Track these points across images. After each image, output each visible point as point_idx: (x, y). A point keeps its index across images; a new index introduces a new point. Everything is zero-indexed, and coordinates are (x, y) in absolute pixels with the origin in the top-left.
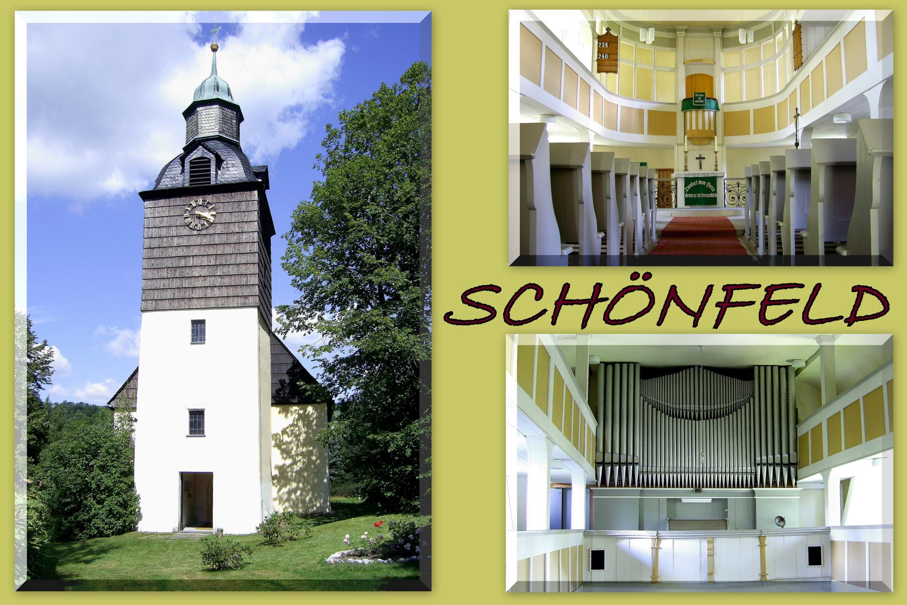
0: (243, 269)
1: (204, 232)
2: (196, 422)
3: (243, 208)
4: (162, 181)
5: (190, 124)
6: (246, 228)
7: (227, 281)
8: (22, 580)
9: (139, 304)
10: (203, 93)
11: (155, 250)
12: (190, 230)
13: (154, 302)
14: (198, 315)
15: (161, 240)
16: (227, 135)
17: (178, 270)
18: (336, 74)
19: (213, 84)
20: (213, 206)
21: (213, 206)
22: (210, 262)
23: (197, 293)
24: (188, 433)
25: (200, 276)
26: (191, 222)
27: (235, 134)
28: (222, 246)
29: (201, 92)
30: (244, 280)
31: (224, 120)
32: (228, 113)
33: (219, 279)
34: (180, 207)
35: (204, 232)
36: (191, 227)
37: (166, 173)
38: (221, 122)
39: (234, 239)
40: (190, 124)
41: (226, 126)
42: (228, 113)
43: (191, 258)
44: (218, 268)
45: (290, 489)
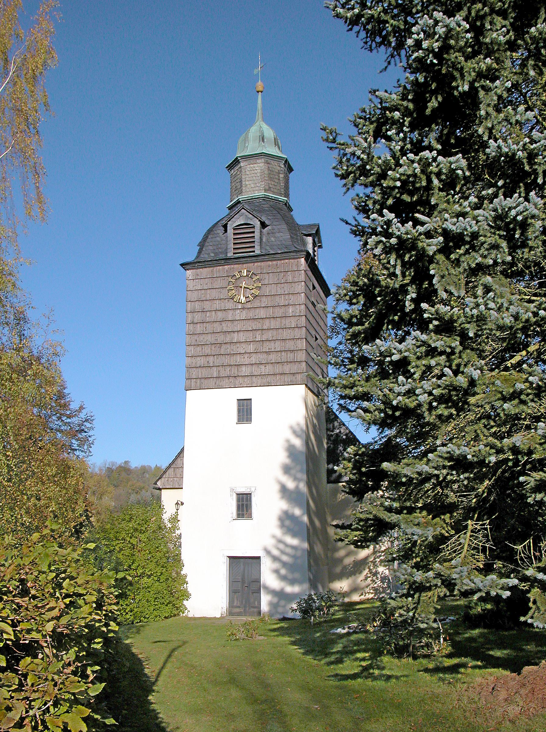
0: (290, 345)
1: (249, 305)
2: (243, 505)
3: (290, 279)
4: (204, 249)
5: (234, 180)
6: (293, 299)
7: (273, 357)
8: (158, 465)
9: (183, 382)
10: (247, 145)
11: (199, 325)
12: (235, 303)
13: (198, 381)
14: (244, 393)
15: (204, 314)
16: (274, 193)
17: (222, 347)
18: (294, 542)
19: (258, 134)
20: (258, 277)
21: (258, 277)
22: (256, 337)
23: (245, 371)
24: (235, 515)
25: (246, 353)
26: (235, 295)
27: (282, 190)
28: (268, 320)
29: (245, 143)
30: (290, 356)
31: (271, 175)
32: (274, 167)
33: (265, 356)
34: (224, 278)
35: (249, 305)
36: (235, 300)
37: (208, 240)
38: (267, 178)
39: (279, 312)
40: (234, 180)
41: (273, 183)
42: (274, 167)
43: (236, 333)
44: (264, 344)
45: (355, 499)
